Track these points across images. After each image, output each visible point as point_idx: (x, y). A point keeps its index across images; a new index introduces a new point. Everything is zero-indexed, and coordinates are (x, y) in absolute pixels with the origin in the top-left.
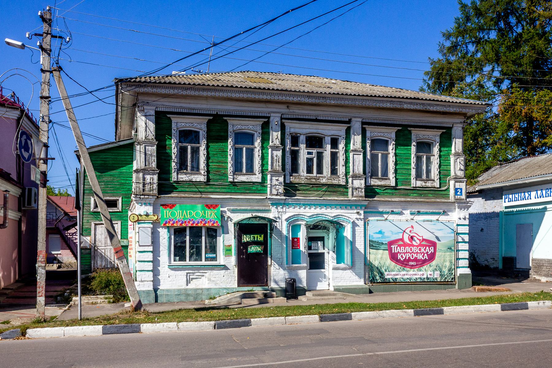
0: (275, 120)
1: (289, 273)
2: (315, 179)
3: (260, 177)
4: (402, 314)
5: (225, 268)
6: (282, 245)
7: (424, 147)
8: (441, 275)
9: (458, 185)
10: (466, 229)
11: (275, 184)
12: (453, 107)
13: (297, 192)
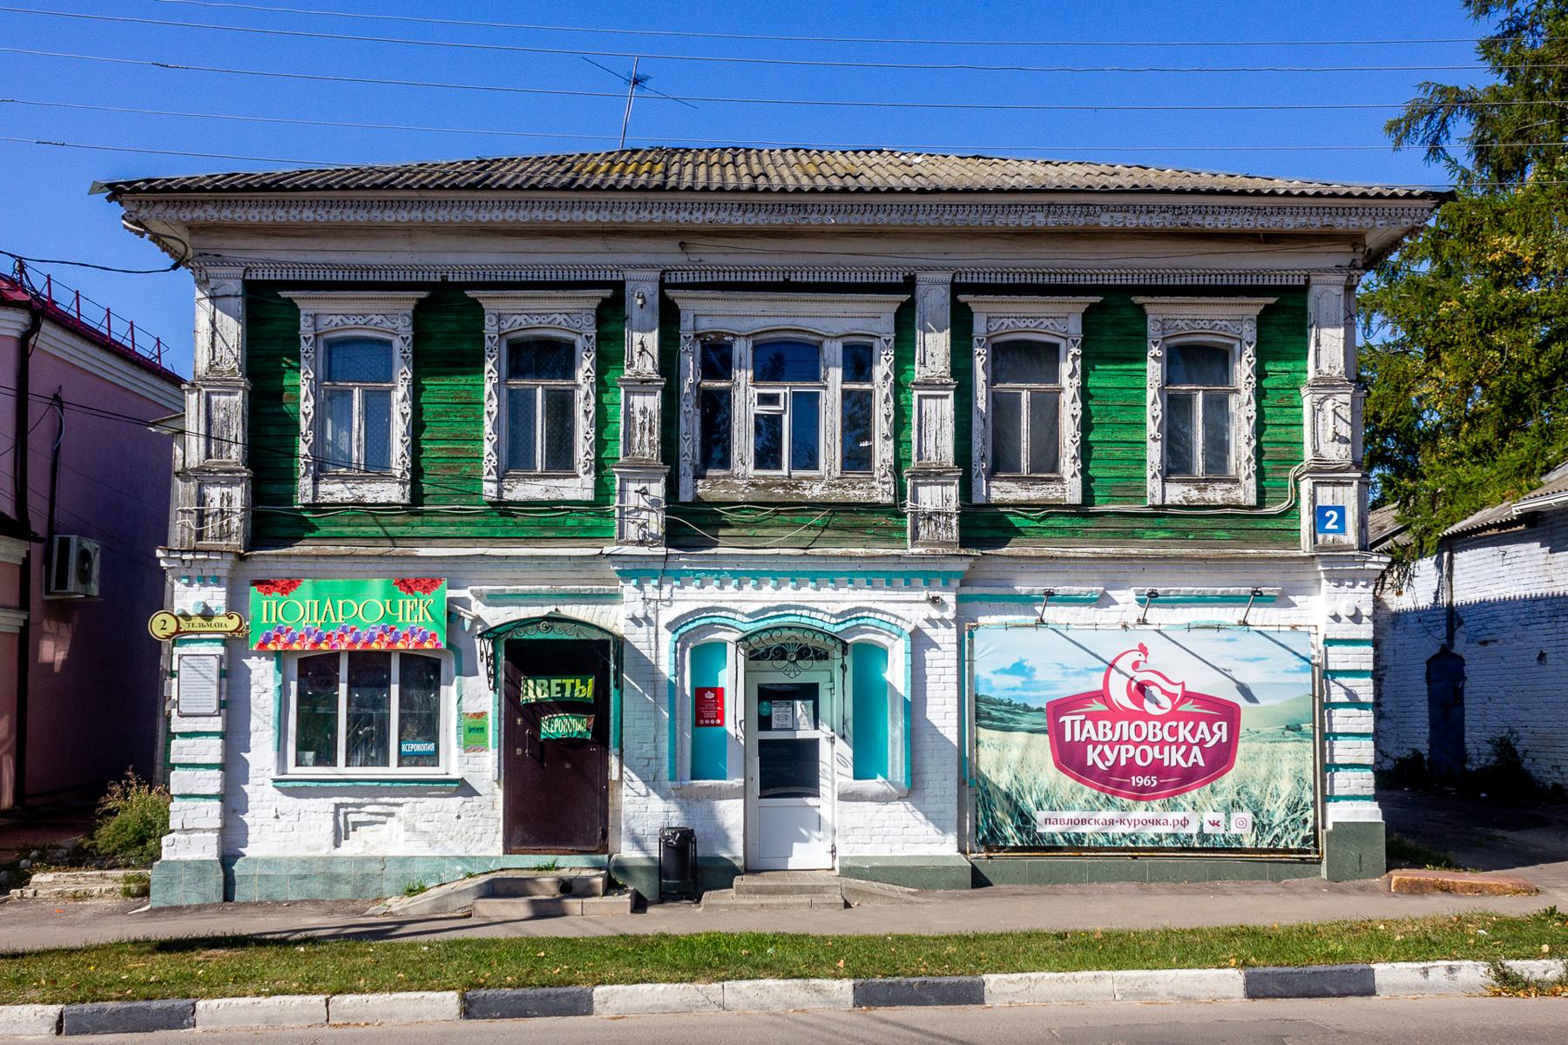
0: (642, 291)
1: (682, 808)
2: (784, 486)
3: (591, 484)
4: (804, 995)
5: (463, 788)
6: (656, 711)
7: (1199, 361)
8: (1260, 827)
9: (1326, 496)
10: (1363, 658)
11: (642, 503)
12: (1295, 212)
13: (722, 532)
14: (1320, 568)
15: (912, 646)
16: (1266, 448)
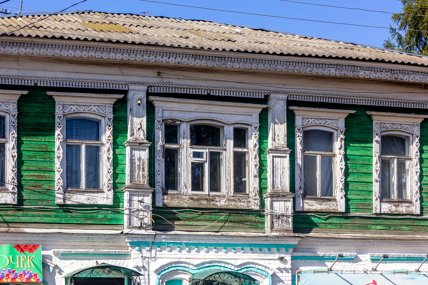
0: (137, 96)
2: (206, 199)
7: (83, 127)
11: (138, 207)
13: (176, 223)
14: (127, 240)
15: (272, 281)
16: (423, 187)
